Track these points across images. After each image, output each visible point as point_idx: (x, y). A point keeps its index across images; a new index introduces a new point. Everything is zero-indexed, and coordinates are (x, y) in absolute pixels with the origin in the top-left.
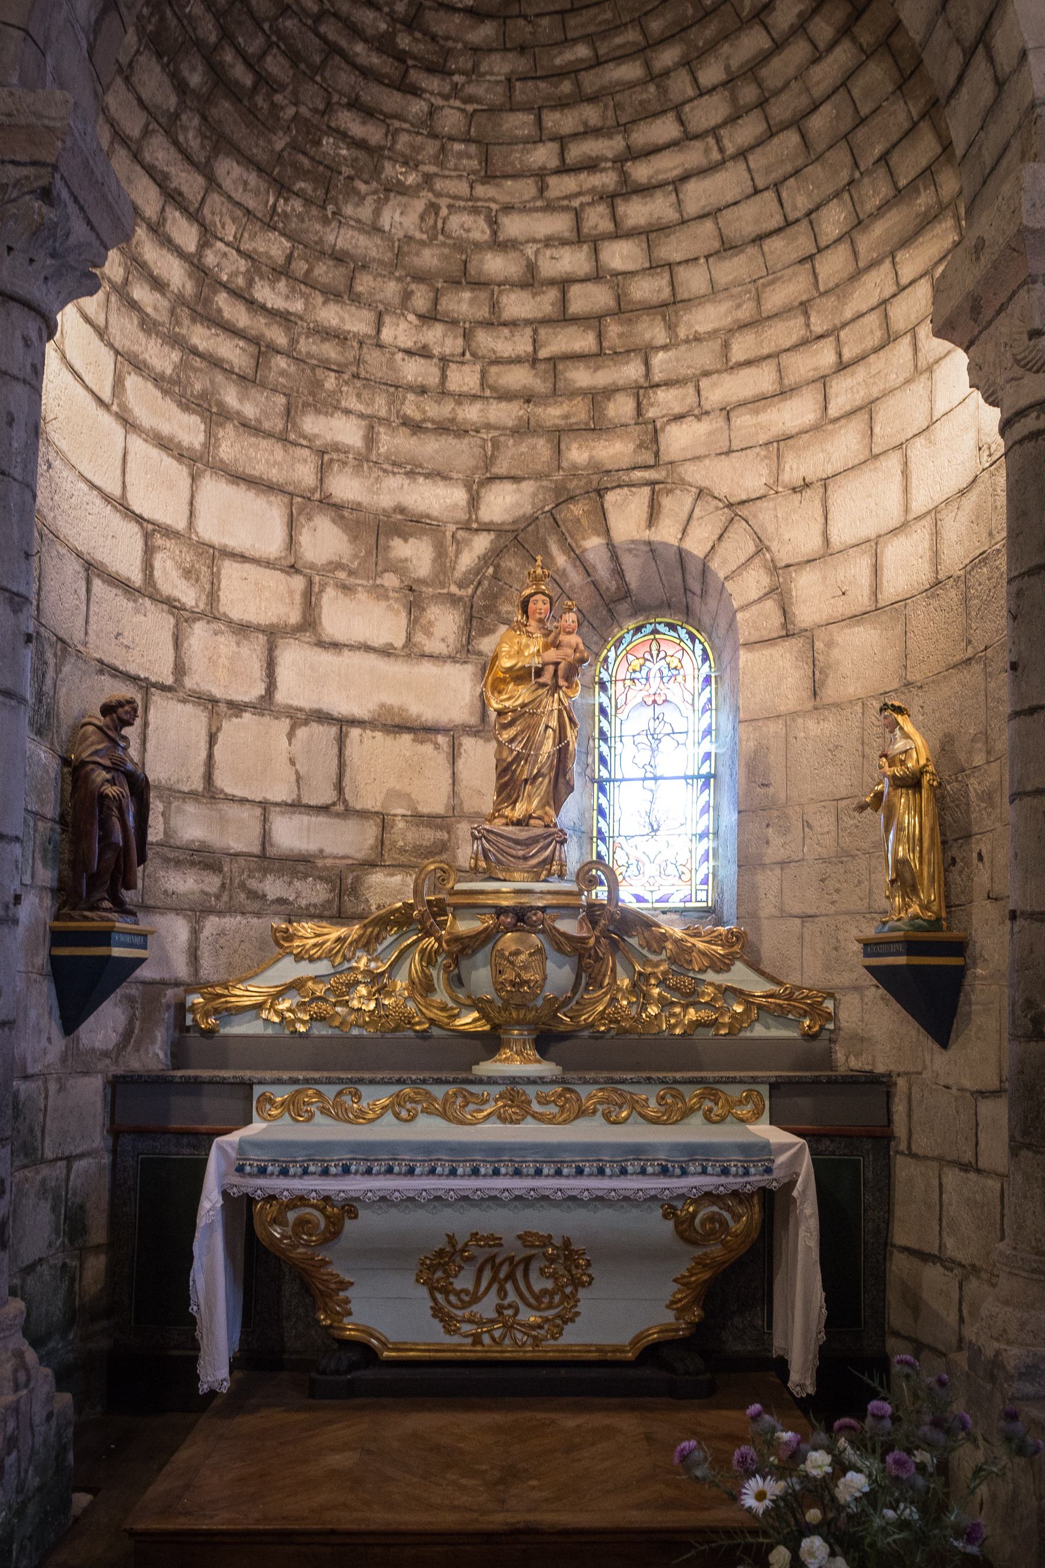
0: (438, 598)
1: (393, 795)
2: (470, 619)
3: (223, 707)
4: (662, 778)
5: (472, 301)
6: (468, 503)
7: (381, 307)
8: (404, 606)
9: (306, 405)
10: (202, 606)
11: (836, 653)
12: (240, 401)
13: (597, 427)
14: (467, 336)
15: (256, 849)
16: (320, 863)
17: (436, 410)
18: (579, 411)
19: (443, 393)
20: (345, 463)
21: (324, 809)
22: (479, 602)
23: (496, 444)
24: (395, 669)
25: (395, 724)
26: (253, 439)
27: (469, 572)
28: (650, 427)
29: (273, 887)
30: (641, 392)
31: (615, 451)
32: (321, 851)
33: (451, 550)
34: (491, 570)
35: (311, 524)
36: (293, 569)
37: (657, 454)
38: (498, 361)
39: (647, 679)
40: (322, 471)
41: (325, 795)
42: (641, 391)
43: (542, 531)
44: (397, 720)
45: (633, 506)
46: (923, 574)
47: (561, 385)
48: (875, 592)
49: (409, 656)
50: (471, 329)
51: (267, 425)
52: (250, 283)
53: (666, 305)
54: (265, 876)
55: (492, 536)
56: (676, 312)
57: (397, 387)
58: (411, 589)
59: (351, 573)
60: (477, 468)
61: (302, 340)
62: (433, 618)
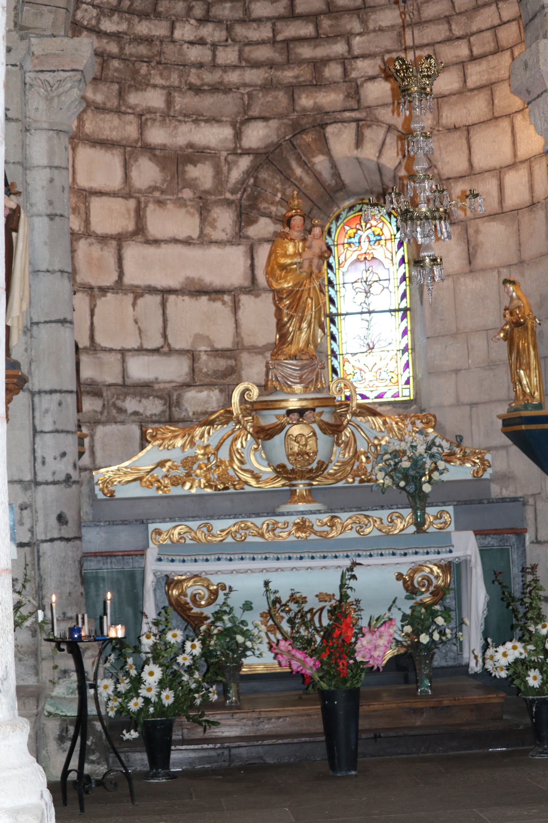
0: (217, 203)
1: (199, 337)
2: (240, 215)
3: (96, 290)
4: (374, 312)
5: (232, 9)
6: (234, 136)
7: (173, 18)
8: (197, 210)
9: (130, 86)
10: (82, 229)
11: (481, 238)
12: (94, 93)
13: (318, 83)
14: (229, 29)
15: (119, 381)
16: (156, 387)
17: (210, 77)
18: (305, 73)
19: (214, 66)
20: (154, 120)
21: (156, 351)
22: (245, 203)
23: (249, 94)
24: (194, 253)
25: (197, 290)
26: (103, 116)
27: (237, 183)
28: (354, 84)
29: (131, 405)
30: (346, 61)
31: (330, 99)
32: (157, 379)
33: (225, 169)
34: (252, 181)
35: (137, 163)
36: (127, 196)
37: (359, 101)
38: (250, 43)
39: (360, 243)
40: (142, 128)
41: (156, 342)
42: (346, 61)
43: (285, 152)
44: (198, 287)
45: (345, 136)
46: (526, 197)
47: (292, 57)
48: (501, 201)
49: (202, 243)
50: (231, 25)
51: (109, 105)
52: (99, 21)
53: (360, 9)
54: (125, 397)
55: (251, 157)
56: (366, 13)
57: (184, 66)
58: (200, 198)
59: (163, 192)
60: (239, 113)
61: (127, 47)
62: (215, 216)
